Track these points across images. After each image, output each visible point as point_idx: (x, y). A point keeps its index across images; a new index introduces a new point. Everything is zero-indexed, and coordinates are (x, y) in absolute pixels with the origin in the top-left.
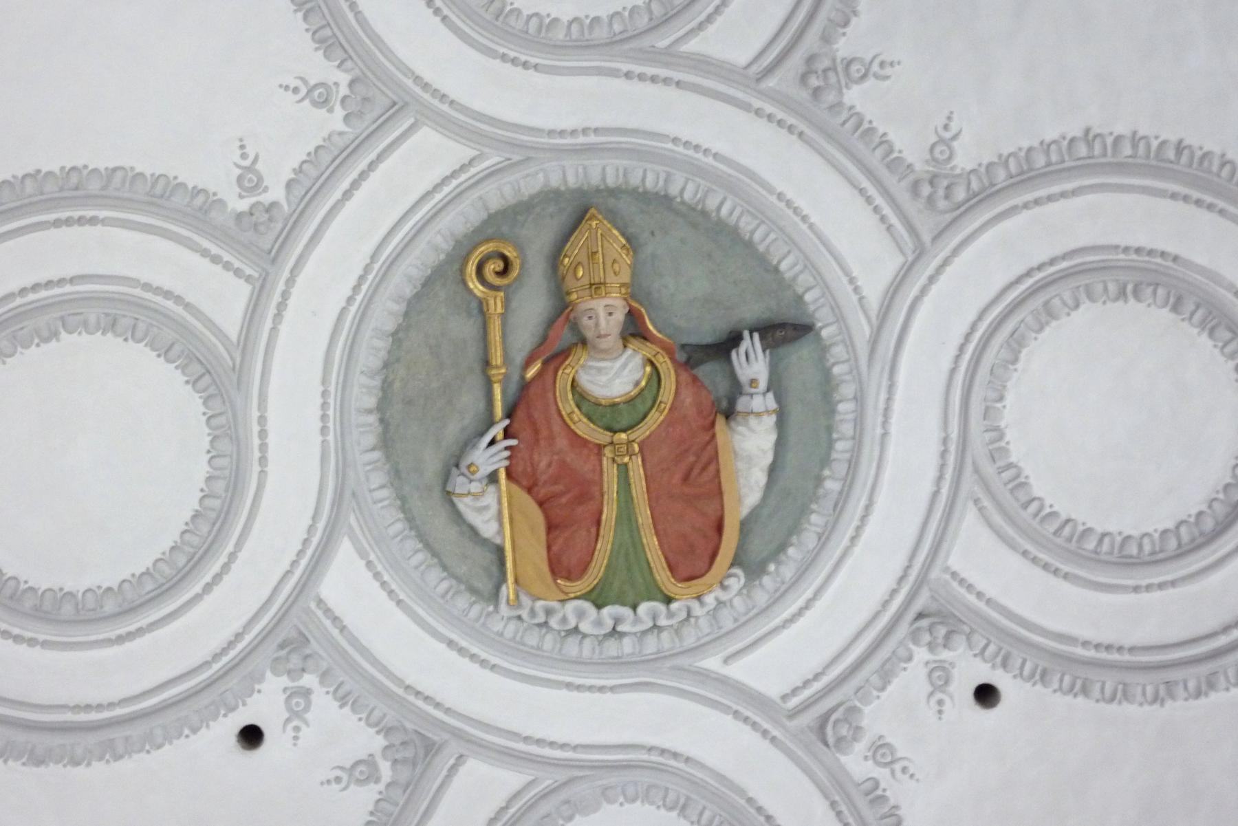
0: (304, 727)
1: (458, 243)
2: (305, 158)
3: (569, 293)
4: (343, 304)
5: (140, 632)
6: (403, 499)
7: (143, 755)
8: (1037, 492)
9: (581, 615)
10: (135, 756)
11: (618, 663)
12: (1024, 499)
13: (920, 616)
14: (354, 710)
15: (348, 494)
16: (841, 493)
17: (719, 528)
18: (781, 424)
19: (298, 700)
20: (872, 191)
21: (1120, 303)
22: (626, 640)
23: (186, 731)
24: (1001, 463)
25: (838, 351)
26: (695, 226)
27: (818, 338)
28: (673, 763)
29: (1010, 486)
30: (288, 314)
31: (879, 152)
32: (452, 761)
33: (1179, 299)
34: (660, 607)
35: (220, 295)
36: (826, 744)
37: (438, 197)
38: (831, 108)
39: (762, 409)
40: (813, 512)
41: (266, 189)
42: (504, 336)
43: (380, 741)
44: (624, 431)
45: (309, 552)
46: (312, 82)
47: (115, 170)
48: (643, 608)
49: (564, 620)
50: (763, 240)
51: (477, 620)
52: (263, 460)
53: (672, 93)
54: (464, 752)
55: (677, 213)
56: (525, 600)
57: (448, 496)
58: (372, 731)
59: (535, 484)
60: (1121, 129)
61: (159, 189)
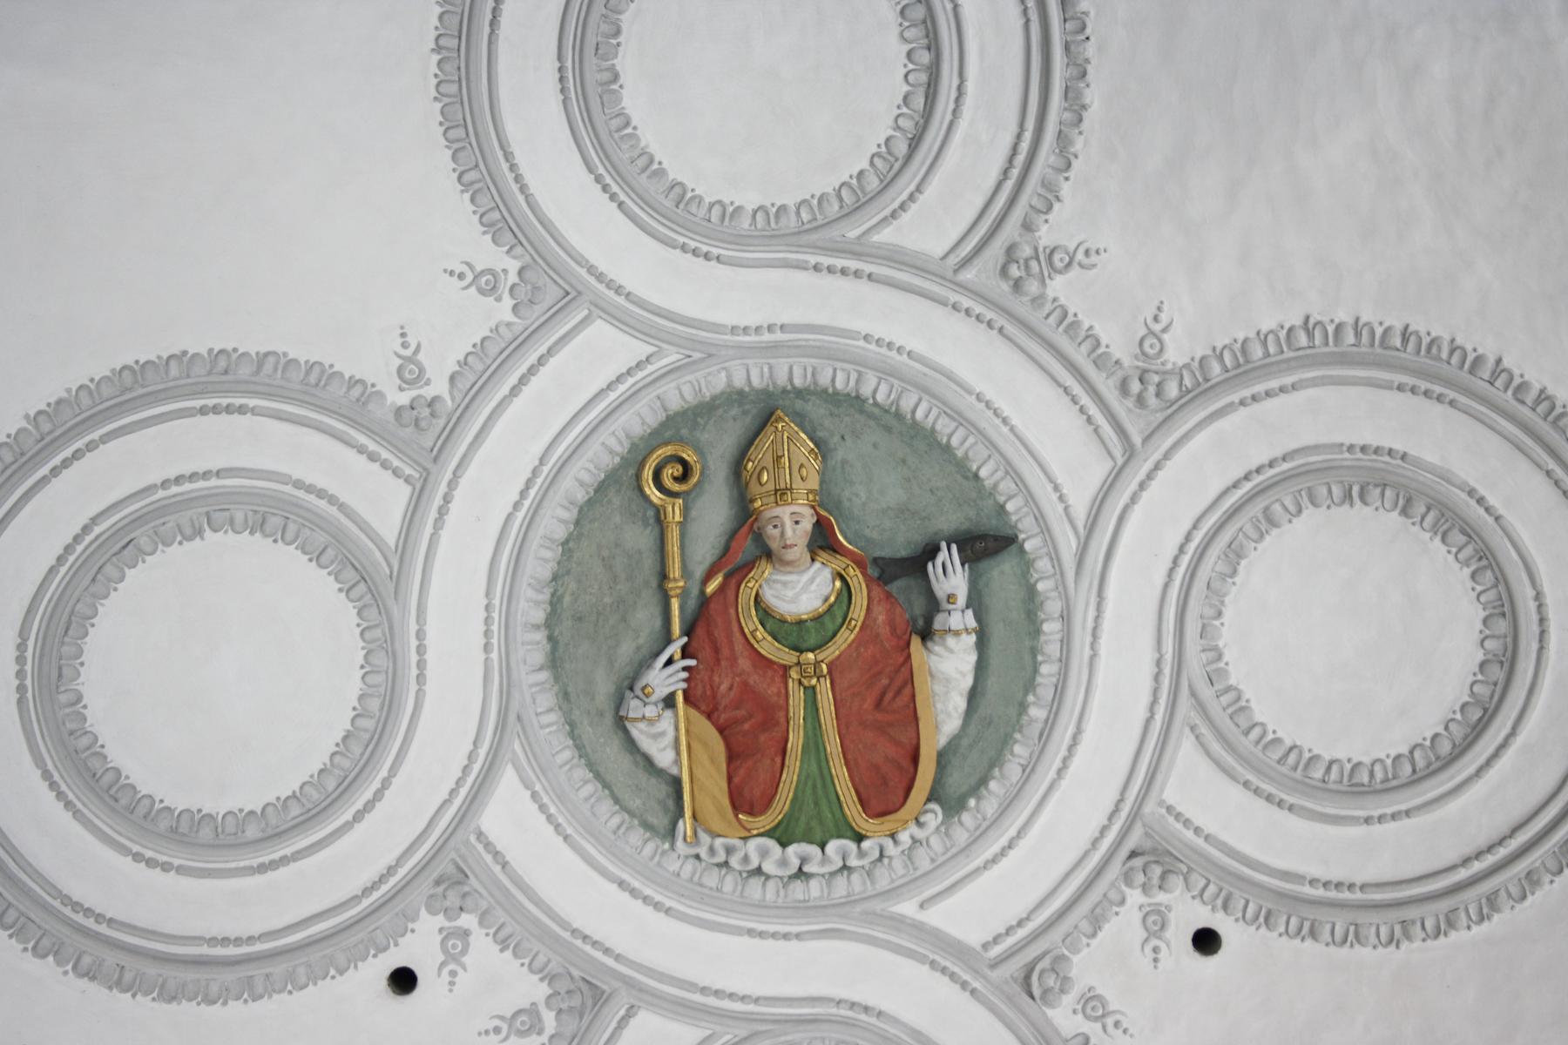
0: (460, 971)
1: (634, 447)
2: (470, 349)
3: (752, 501)
4: (510, 509)
5: (284, 861)
6: (572, 725)
7: (285, 996)
8: (1259, 718)
9: (764, 853)
10: (275, 996)
11: (804, 909)
12: (1244, 725)
13: (1133, 854)
14: (515, 955)
15: (512, 718)
16: (1046, 721)
17: (915, 758)
18: (982, 644)
19: (455, 944)
20: (1077, 389)
21: (1346, 507)
22: (813, 883)
23: (332, 972)
24: (1218, 686)
25: (1043, 565)
26: (888, 429)
27: (1022, 550)
28: (863, 1017)
29: (1230, 711)
30: (450, 519)
31: (1085, 348)
32: (622, 1012)
33: (1409, 501)
34: (851, 845)
35: (376, 497)
36: (1032, 997)
37: (613, 396)
38: (1034, 300)
39: (961, 627)
40: (1016, 741)
41: (428, 383)
42: (682, 547)
43: (544, 990)
44: (812, 651)
45: (470, 780)
46: (479, 269)
47: (267, 354)
48: (833, 846)
49: (746, 859)
50: (962, 443)
51: (652, 858)
52: (421, 678)
53: (864, 287)
54: (636, 1003)
55: (870, 416)
56: (705, 838)
57: (621, 722)
58: (536, 978)
59: (715, 709)
60: (1343, 315)
61: (313, 379)
